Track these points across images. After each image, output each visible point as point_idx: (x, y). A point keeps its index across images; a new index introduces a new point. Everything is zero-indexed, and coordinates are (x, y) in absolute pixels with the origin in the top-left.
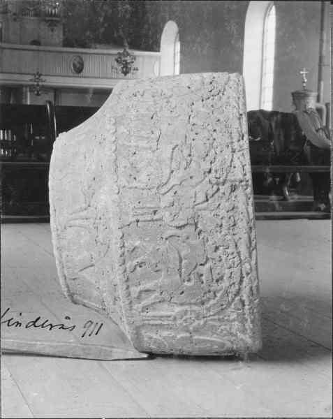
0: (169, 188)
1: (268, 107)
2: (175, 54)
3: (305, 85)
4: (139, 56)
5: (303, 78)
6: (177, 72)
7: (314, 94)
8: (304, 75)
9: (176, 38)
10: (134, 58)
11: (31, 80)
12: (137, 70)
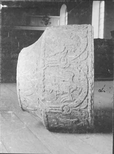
1: (102, 37)
4: (51, 18)
9: (66, 11)
10: (50, 18)
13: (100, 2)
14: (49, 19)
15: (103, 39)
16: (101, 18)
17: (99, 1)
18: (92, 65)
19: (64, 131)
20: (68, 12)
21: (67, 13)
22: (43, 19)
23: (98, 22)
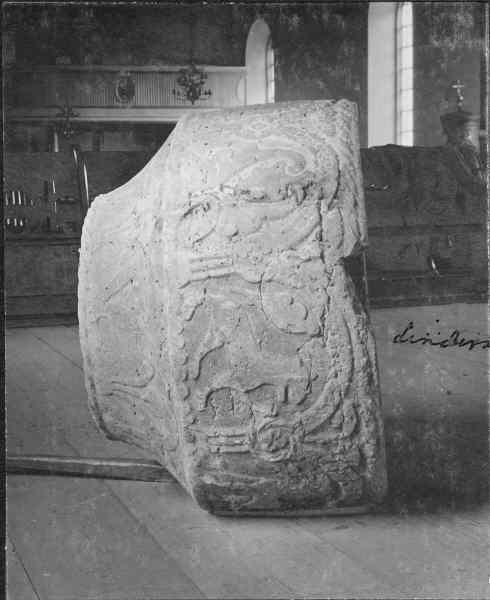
0: (237, 433)
1: (407, 140)
2: (266, 69)
3: (460, 104)
4: (210, 73)
5: (3, 309)
6: (272, 100)
7: (477, 117)
8: (459, 91)
9: (268, 44)
10: (204, 76)
11: (58, 116)
12: (210, 93)
13: (397, 8)
14: (202, 78)
15: (414, 147)
16: (404, 108)
17: (391, 5)
18: (361, 224)
19: (420, 506)
20: (274, 47)
21: (271, 55)
22: (179, 81)
23: (393, 63)
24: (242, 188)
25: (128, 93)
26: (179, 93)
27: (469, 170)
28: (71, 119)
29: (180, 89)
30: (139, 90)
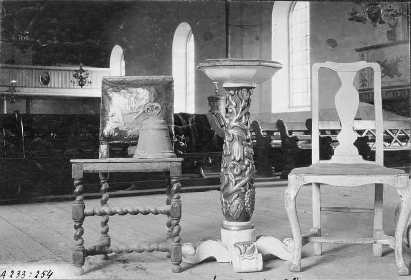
8: (216, 84)
12: (91, 83)
24: (238, 270)
25: (46, 82)
26: (74, 83)
27: (219, 126)
28: (14, 93)
29: (75, 80)
30: (53, 79)
